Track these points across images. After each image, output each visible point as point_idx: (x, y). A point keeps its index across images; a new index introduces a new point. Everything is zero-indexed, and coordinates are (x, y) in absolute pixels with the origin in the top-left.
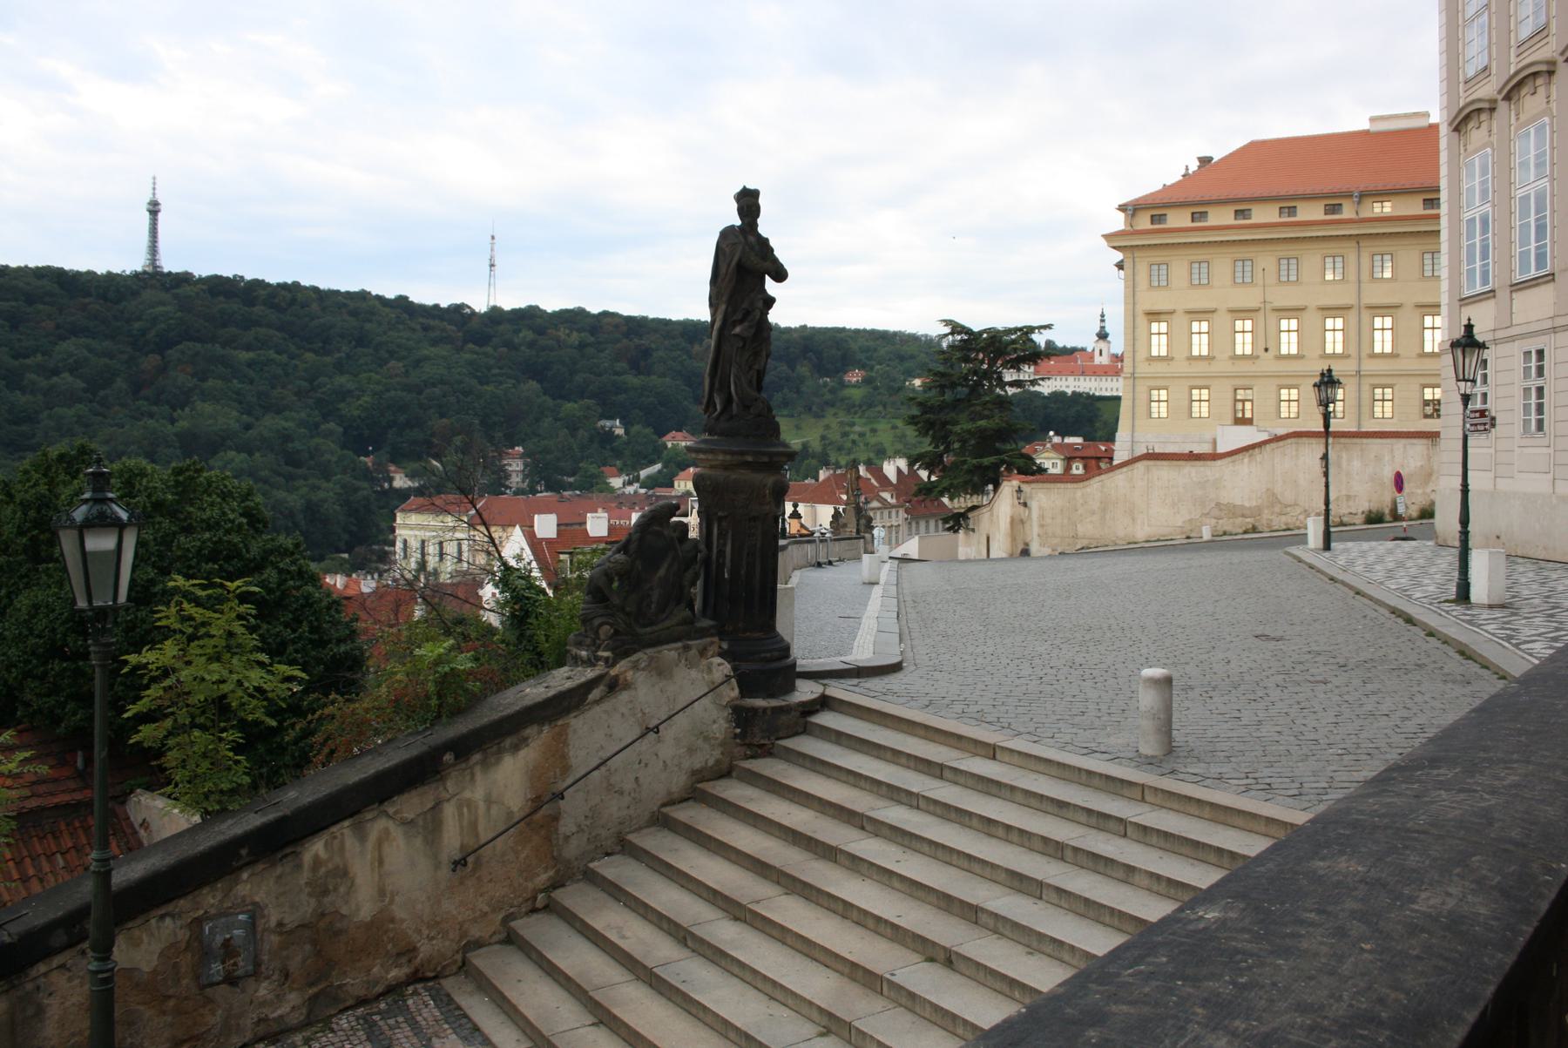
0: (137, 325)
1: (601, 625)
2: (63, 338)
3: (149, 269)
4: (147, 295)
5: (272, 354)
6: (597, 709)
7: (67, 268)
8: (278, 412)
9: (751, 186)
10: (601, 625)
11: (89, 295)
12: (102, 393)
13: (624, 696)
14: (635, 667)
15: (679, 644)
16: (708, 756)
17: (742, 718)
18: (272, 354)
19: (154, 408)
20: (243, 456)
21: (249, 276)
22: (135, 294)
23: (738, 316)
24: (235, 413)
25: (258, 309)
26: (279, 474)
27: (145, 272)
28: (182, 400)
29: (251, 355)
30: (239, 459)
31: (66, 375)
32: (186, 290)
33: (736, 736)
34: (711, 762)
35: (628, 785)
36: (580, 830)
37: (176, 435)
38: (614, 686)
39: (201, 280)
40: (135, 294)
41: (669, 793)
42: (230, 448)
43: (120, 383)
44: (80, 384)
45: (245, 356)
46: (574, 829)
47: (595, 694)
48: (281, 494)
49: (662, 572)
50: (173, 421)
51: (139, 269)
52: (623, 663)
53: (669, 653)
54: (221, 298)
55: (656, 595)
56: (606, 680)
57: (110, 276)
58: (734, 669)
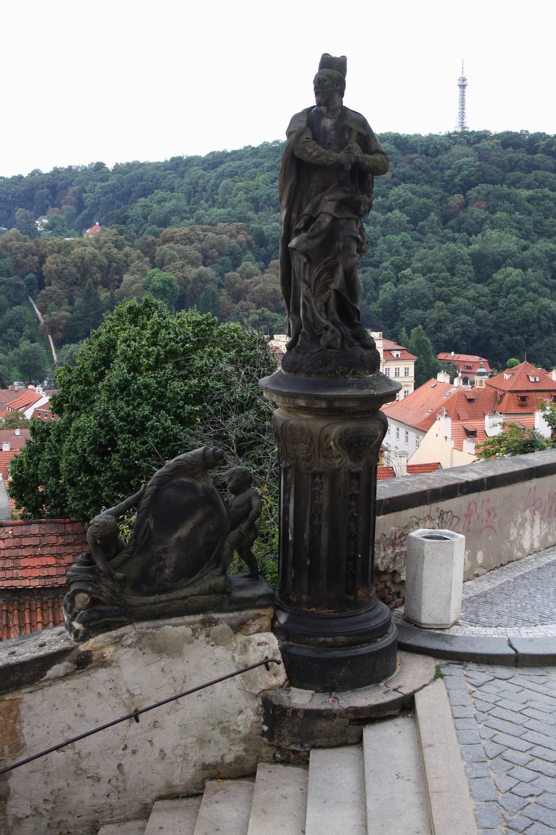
0: (448, 173)
1: (76, 592)
2: (396, 185)
3: (459, 130)
4: (456, 149)
5: (547, 191)
6: (62, 686)
7: (401, 133)
8: (549, 237)
9: (336, 54)
10: (76, 592)
11: (415, 151)
12: (420, 224)
13: (102, 674)
14: (118, 642)
15: (200, 617)
16: (226, 751)
17: (273, 713)
18: (547, 191)
19: (457, 235)
20: (519, 271)
21: (532, 131)
22: (447, 149)
23: (301, 225)
24: (514, 238)
25: (539, 156)
26: (546, 286)
27: (455, 133)
28: (476, 228)
29: (531, 192)
30: (515, 273)
31: (397, 211)
32: (484, 144)
33: (263, 734)
34: (229, 758)
35: (108, 770)
36: (37, 812)
37: (470, 255)
38: (84, 663)
39: (497, 136)
40: (447, 149)
41: (169, 785)
42: (509, 265)
43: (433, 216)
44: (406, 218)
45: (525, 193)
46: (28, 812)
47: (57, 669)
48: (546, 301)
49: (183, 532)
50: (469, 244)
51: (452, 131)
52: (101, 637)
53: (174, 629)
54: (510, 149)
55: (171, 559)
56: (73, 655)
57: (431, 138)
58: (283, 650)
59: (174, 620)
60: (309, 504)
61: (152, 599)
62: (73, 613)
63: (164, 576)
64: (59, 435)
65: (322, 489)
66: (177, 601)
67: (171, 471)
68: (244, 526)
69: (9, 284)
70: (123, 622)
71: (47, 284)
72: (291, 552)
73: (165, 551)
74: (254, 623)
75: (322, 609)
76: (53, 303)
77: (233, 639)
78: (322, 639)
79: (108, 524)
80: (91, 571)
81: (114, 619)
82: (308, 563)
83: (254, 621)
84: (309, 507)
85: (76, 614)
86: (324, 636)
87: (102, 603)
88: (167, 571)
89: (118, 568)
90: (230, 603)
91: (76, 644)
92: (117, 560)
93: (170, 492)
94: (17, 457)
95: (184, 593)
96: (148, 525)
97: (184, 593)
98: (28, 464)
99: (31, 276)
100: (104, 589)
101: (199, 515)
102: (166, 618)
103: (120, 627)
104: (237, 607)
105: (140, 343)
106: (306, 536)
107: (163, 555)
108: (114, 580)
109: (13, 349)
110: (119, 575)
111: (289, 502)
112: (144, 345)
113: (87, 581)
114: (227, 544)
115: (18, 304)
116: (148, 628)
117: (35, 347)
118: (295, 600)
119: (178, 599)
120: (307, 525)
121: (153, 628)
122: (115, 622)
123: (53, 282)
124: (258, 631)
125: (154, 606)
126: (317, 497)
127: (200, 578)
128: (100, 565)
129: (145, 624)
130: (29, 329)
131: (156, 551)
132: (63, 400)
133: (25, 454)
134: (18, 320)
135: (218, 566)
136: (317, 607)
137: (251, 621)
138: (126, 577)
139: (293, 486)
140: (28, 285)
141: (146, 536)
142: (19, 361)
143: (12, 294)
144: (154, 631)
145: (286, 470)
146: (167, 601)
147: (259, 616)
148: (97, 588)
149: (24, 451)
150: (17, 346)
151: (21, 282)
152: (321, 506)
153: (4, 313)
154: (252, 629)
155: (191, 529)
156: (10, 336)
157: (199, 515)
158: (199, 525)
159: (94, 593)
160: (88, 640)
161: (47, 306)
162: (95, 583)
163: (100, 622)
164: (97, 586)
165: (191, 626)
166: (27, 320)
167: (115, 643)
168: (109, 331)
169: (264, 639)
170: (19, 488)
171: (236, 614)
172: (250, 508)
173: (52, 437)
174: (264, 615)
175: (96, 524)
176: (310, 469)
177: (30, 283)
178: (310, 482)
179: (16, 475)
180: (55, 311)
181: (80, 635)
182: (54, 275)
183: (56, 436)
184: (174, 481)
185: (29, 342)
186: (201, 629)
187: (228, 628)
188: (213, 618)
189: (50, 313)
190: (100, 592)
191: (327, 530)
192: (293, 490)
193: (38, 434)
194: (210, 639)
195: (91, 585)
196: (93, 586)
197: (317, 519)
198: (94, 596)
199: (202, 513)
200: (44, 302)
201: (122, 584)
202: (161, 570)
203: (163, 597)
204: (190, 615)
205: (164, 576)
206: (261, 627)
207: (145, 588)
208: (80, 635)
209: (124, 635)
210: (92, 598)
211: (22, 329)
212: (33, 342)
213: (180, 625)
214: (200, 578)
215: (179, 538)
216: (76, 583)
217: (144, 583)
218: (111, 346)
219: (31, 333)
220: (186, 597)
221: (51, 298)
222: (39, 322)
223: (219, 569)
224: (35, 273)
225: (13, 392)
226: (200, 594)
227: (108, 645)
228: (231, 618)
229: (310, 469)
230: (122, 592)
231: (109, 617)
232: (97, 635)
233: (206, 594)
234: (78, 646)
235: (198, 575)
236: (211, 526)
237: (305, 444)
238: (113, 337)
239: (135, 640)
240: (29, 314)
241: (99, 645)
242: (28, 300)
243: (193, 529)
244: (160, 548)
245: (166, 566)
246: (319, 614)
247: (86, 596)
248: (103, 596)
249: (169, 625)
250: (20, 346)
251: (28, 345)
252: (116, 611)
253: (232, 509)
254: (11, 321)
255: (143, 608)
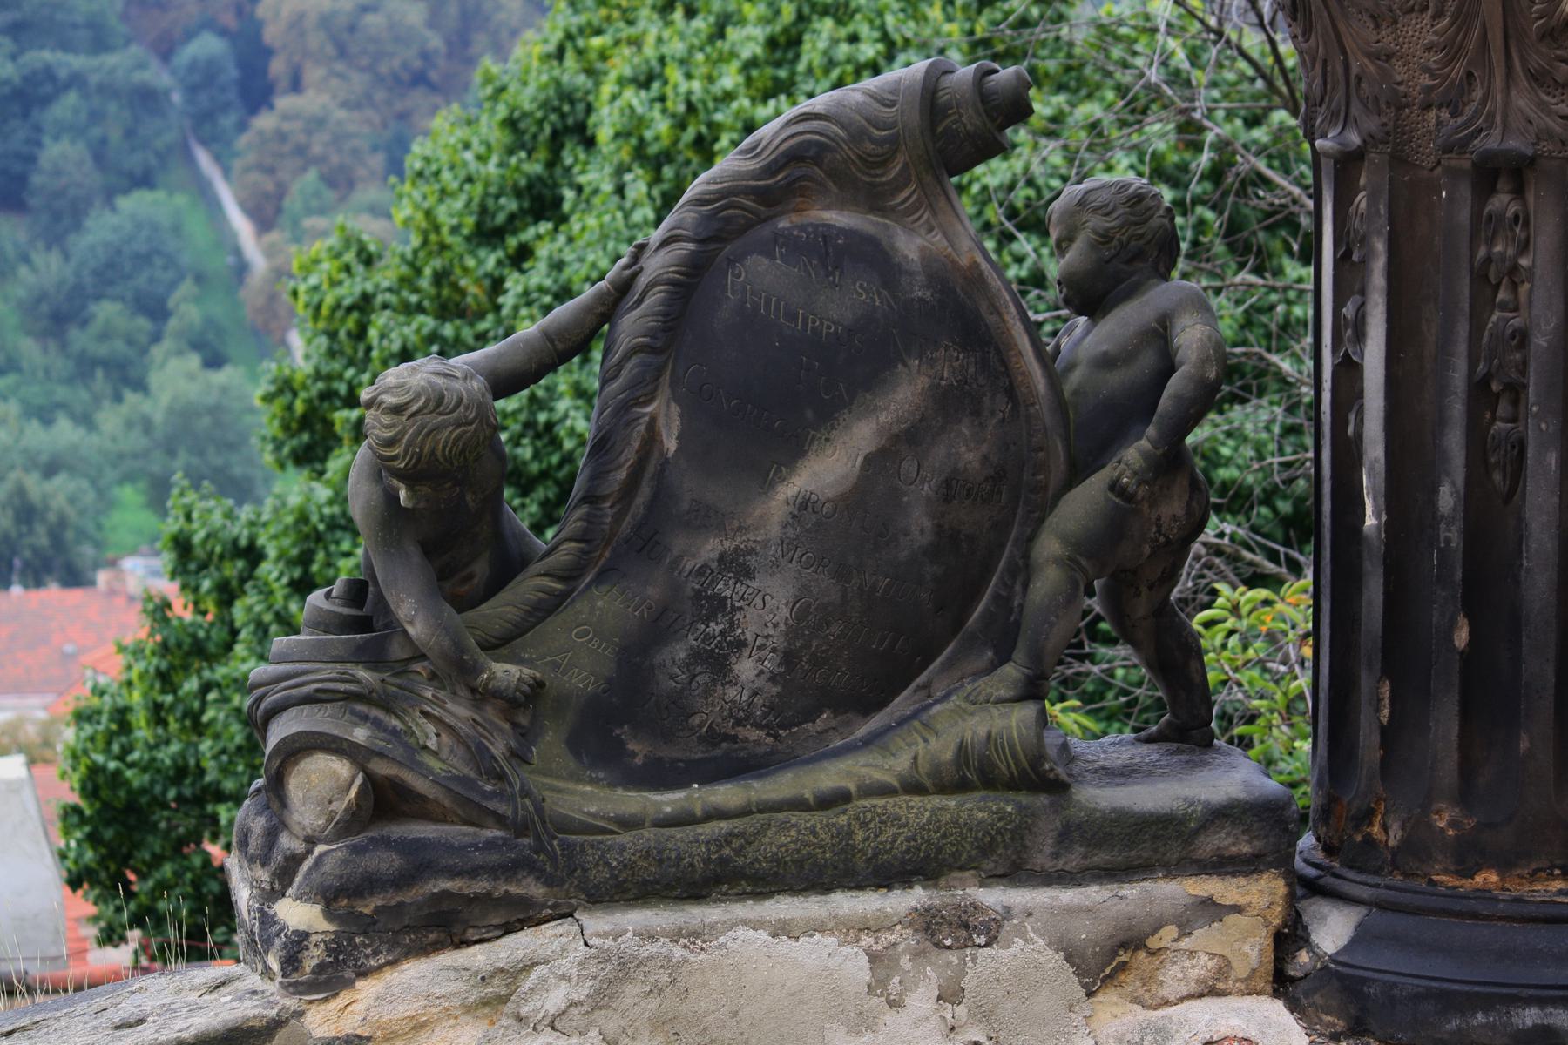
15: (917, 897)
49: (827, 469)
55: (768, 608)
59: (783, 907)
60: (1463, 330)
61: (668, 801)
62: (278, 857)
63: (732, 693)
64: (305, 559)
65: (1524, 247)
66: (794, 817)
67: (770, 170)
68: (1134, 454)
69: (102, 89)
70: (525, 902)
71: (284, 83)
72: (1374, 591)
73: (737, 565)
74: (1185, 943)
75: (1533, 876)
76: (312, 175)
77: (1077, 1018)
78: (1530, 1017)
79: (451, 400)
80: (373, 657)
81: (481, 886)
82: (1462, 637)
83: (1185, 930)
84: (1462, 348)
85: (294, 861)
86: (1541, 1002)
87: (419, 808)
88: (745, 668)
89: (497, 645)
90: (1065, 837)
91: (291, 1003)
92: (502, 608)
93: (760, 274)
94: (102, 693)
95: (829, 776)
96: (652, 437)
97: (829, 776)
98: (158, 714)
99: (207, 46)
100: (428, 733)
101: (905, 394)
102: (742, 896)
103: (508, 929)
104: (1101, 858)
105: (710, 79)
106: (1447, 499)
107: (724, 588)
108: (481, 696)
109: (118, 398)
110: (505, 672)
111: (1360, 336)
112: (728, 96)
113: (349, 697)
114: (1049, 546)
115: (144, 180)
116: (649, 936)
117: (224, 390)
118: (1394, 837)
119: (798, 804)
120: (1455, 442)
121: (676, 935)
122: (486, 900)
123: (313, 74)
124: (1210, 990)
125: (678, 833)
126: (1502, 295)
127: (915, 715)
128: (414, 615)
129: (634, 919)
130: (197, 300)
131: (690, 564)
132: (327, 395)
133: (139, 666)
134: (144, 259)
135: (1003, 658)
136: (1504, 865)
137: (1169, 932)
138: (539, 685)
139: (1380, 246)
140: (192, 90)
141: (645, 492)
142: (144, 455)
143: (115, 136)
144: (678, 952)
145: (1347, 165)
146: (745, 812)
147: (1211, 910)
148: (394, 732)
149: (138, 652)
150: (141, 386)
151: (158, 76)
152: (1522, 338)
153: (77, 226)
154: (1176, 976)
155: (869, 460)
156: (105, 336)
157: (905, 394)
158: (906, 440)
159: (381, 755)
160: (349, 984)
161: (281, 192)
162: (389, 710)
163: (410, 896)
164: (395, 722)
165: (867, 940)
166: (186, 259)
167: (485, 1003)
168: (560, 54)
169: (1235, 1022)
170: (108, 834)
171: (1095, 894)
172: (1168, 367)
173: (269, 570)
174: (1238, 909)
175: (390, 400)
176: (1464, 144)
177: (203, 78)
178: (1464, 215)
179: (95, 770)
180: (322, 211)
181: (312, 958)
182: (315, 40)
183: (291, 563)
184: (783, 224)
185: (194, 361)
186: (917, 955)
187: (1054, 960)
188: (977, 907)
189: (295, 223)
190: (413, 752)
191: (1552, 459)
192: (1379, 266)
193: (204, 566)
194: (961, 1010)
195: (364, 718)
196: (377, 724)
197: (1503, 408)
198: (382, 768)
199: (923, 382)
200: (271, 171)
201: (523, 720)
202: (717, 662)
203: (727, 794)
204: (860, 887)
205: (732, 693)
206: (1224, 970)
207: (639, 749)
208: (312, 958)
209: (528, 967)
210: (370, 778)
211: (162, 302)
212: (214, 361)
213: (818, 927)
214: (915, 715)
215: (805, 503)
216: (294, 711)
217: (628, 721)
218: (568, 125)
219: (209, 322)
220: (838, 799)
221: (301, 150)
222: (242, 269)
223: (1012, 671)
224: (223, 32)
225: (120, 602)
226: (913, 787)
227: (448, 1014)
228: (1070, 910)
229: (1464, 144)
230: (519, 756)
231: (453, 873)
232: (393, 963)
233: (943, 789)
234: (300, 1014)
235: (901, 704)
236: (966, 449)
237: (1438, 15)
238: (571, 73)
239: (582, 992)
240: (197, 227)
241: (404, 1010)
242: (190, 160)
243: (879, 462)
244: (710, 548)
245: (741, 644)
246: (1518, 900)
247: (342, 768)
248: (424, 771)
249: (756, 925)
250: (154, 379)
251: (191, 377)
252: (491, 845)
253: (1076, 377)
254: (110, 265)
255: (626, 838)
